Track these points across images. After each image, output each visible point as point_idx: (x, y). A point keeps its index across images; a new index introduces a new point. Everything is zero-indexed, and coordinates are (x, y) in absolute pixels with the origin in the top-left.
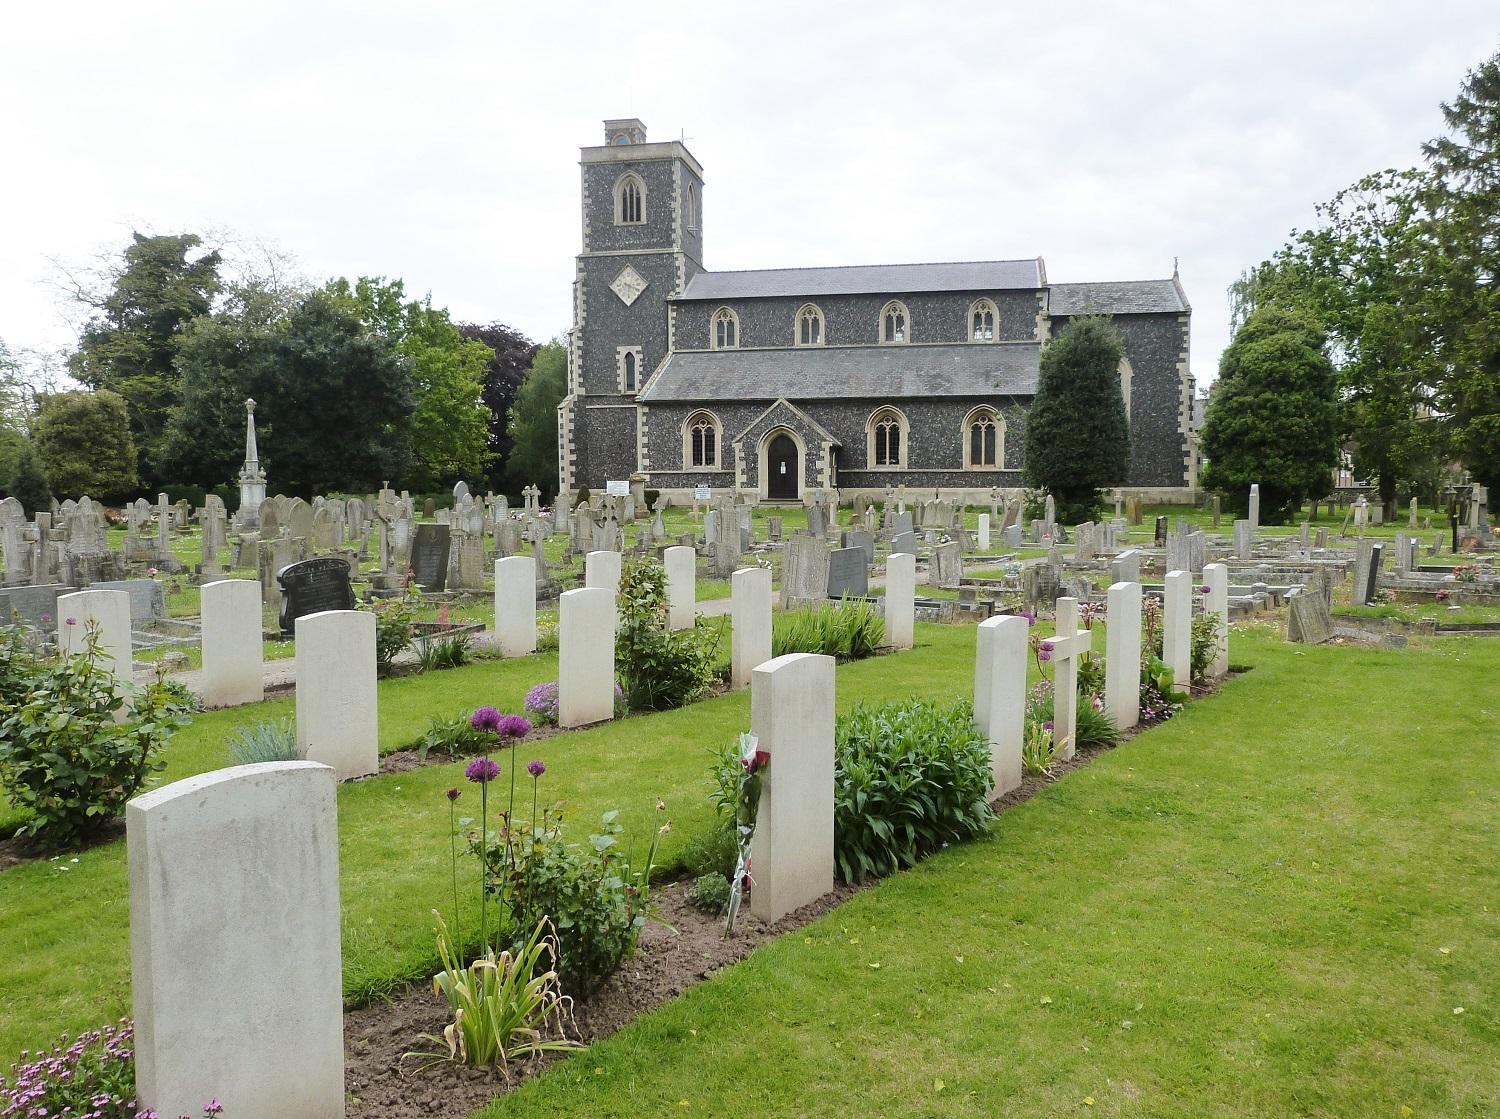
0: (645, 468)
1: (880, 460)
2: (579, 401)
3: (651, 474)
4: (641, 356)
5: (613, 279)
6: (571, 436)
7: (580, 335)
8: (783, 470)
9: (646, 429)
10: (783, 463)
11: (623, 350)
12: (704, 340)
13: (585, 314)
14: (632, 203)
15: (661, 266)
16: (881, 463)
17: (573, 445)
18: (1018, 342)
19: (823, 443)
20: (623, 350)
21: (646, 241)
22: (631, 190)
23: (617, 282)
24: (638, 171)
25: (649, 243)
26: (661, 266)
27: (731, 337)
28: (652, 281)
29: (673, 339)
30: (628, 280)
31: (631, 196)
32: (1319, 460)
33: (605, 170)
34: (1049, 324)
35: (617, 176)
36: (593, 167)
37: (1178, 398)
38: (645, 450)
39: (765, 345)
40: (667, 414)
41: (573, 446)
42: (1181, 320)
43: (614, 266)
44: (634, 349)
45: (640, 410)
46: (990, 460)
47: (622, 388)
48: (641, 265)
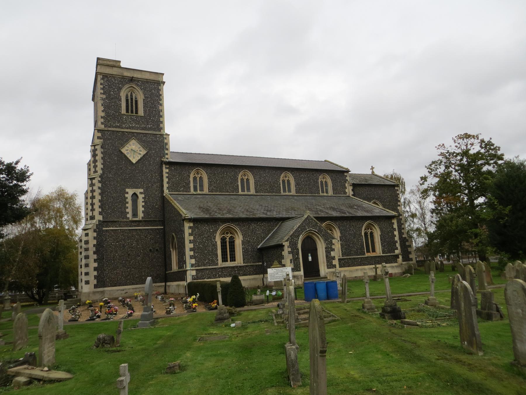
0: (192, 265)
1: (224, 259)
2: (99, 224)
3: (196, 270)
4: (143, 196)
5: (123, 146)
6: (94, 249)
7: (100, 179)
8: (310, 258)
9: (192, 238)
10: (310, 254)
11: (130, 192)
12: (187, 188)
13: (102, 166)
14: (132, 103)
15: (156, 141)
16: (225, 261)
17: (96, 255)
18: (340, 195)
19: (333, 240)
20: (130, 192)
21: (143, 126)
22: (131, 95)
23: (126, 148)
24: (138, 85)
25: (146, 127)
26: (156, 141)
27: (202, 186)
28: (150, 149)
29: (167, 185)
30: (133, 147)
31: (132, 99)
32: (461, 243)
33: (115, 80)
34: (351, 188)
35: (123, 85)
36: (107, 76)
37: (401, 222)
38: (192, 253)
39: (223, 192)
40: (205, 228)
41: (95, 257)
42: (396, 188)
43: (125, 139)
44: (138, 191)
45: (187, 225)
46: (233, 259)
47: (130, 216)
48: (142, 140)
